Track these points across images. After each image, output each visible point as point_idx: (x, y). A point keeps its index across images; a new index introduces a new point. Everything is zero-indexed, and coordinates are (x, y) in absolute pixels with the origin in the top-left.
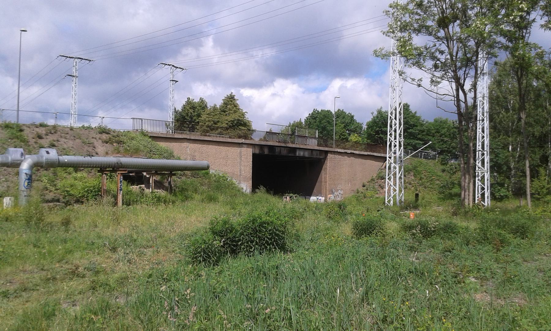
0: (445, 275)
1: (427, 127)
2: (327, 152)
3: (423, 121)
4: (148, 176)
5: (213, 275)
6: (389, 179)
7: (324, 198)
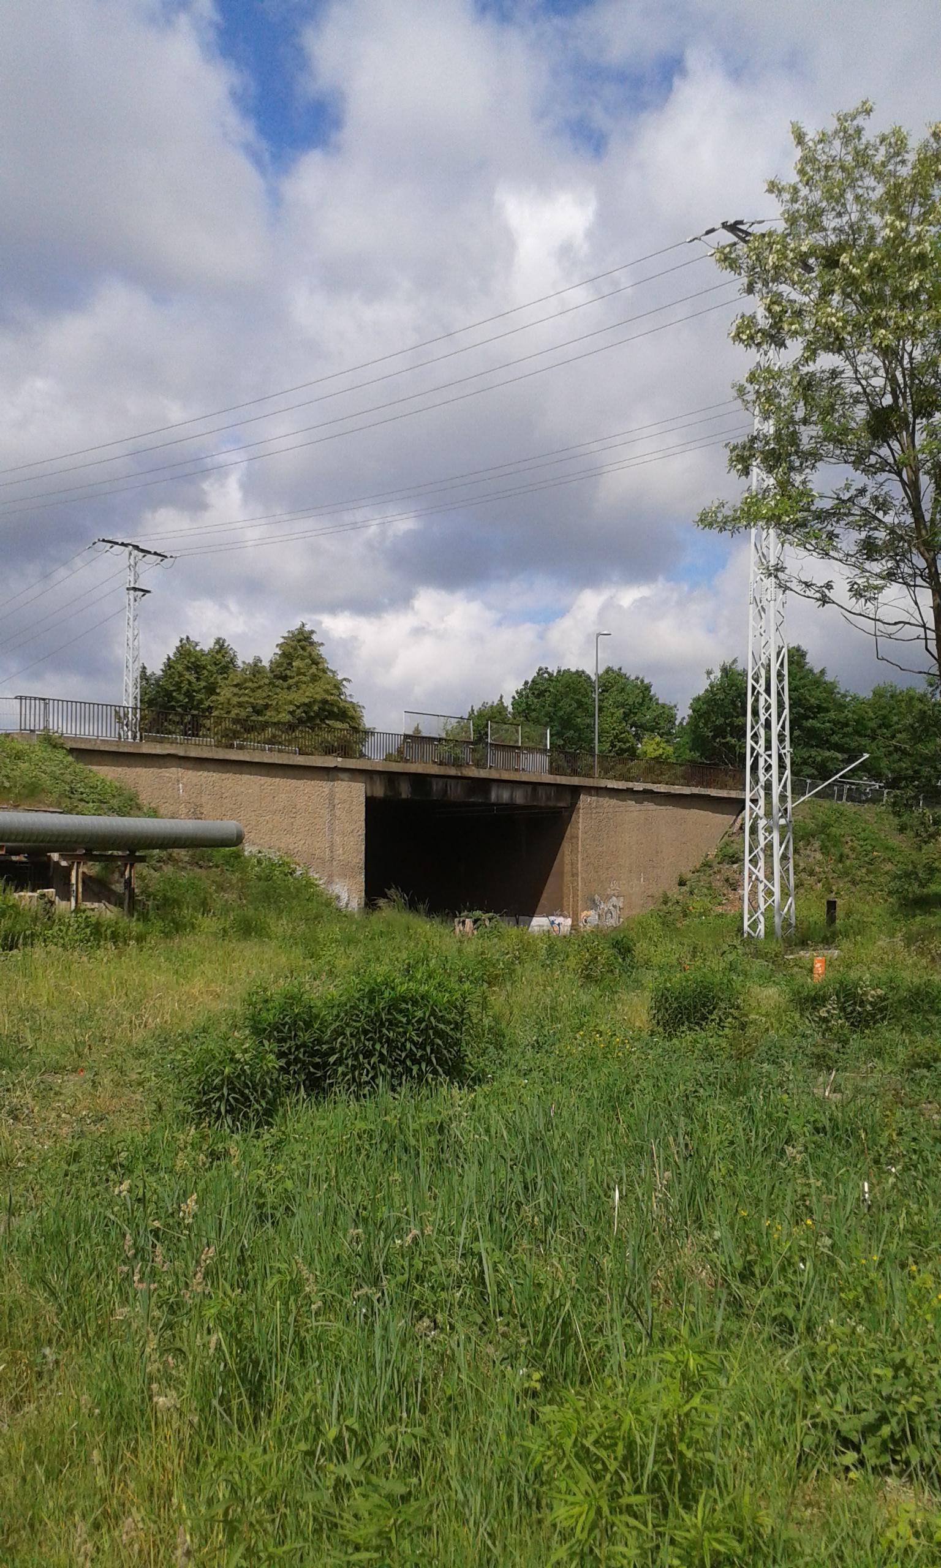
0: (916, 1135)
1: (854, 712)
2: (576, 791)
3: (844, 696)
4: (64, 863)
5: (257, 1154)
6: (754, 861)
7: (569, 921)
